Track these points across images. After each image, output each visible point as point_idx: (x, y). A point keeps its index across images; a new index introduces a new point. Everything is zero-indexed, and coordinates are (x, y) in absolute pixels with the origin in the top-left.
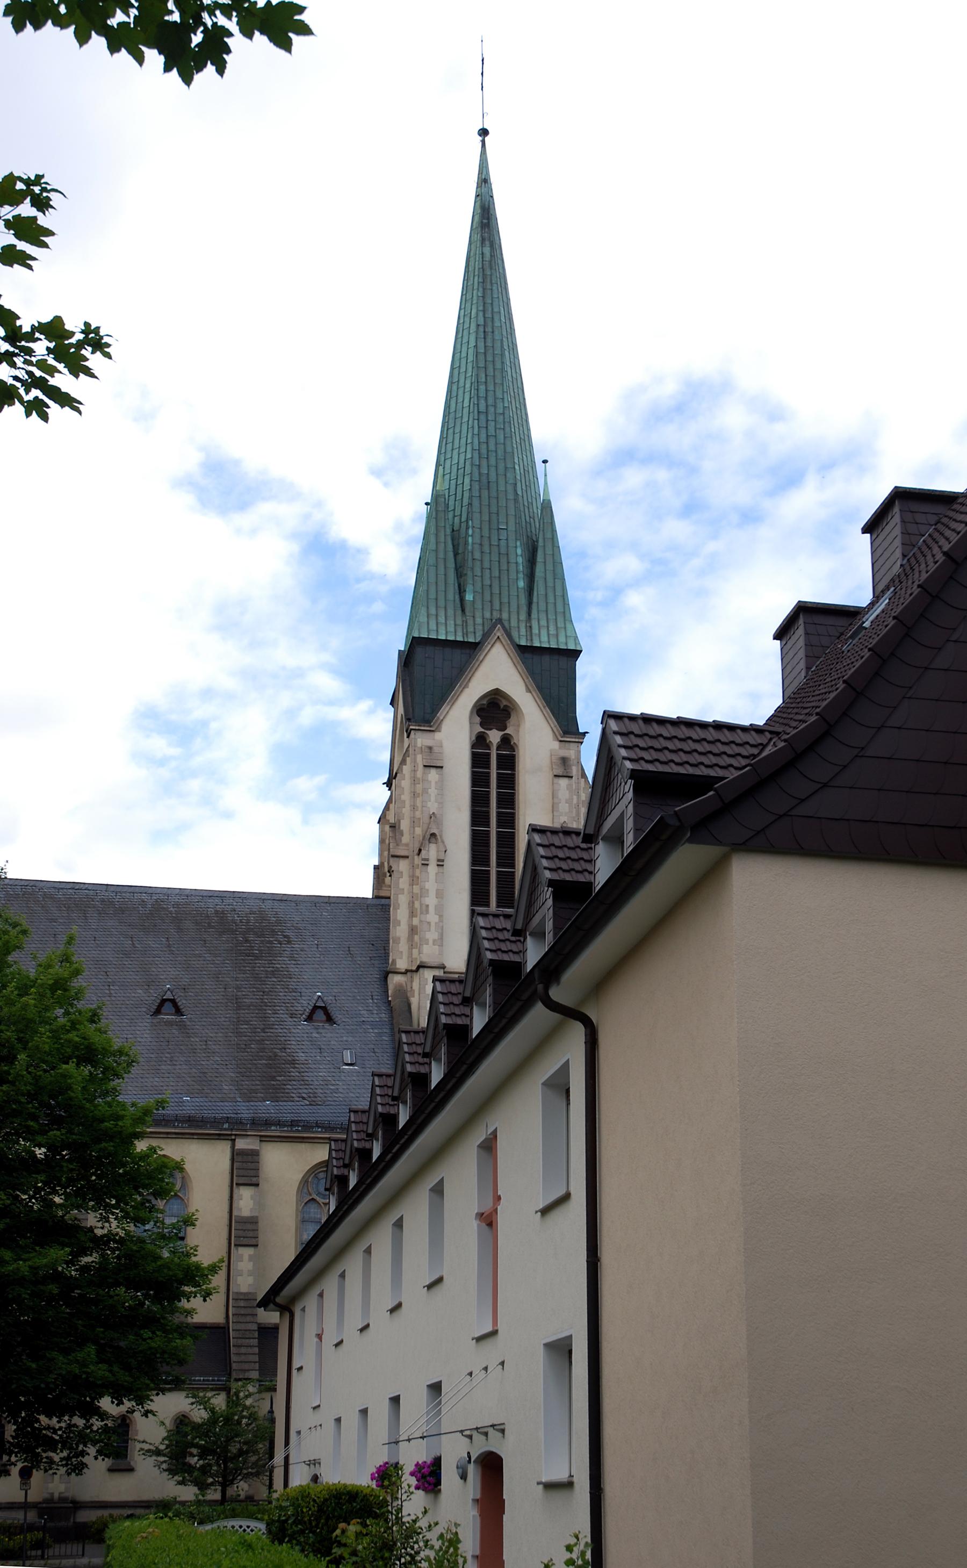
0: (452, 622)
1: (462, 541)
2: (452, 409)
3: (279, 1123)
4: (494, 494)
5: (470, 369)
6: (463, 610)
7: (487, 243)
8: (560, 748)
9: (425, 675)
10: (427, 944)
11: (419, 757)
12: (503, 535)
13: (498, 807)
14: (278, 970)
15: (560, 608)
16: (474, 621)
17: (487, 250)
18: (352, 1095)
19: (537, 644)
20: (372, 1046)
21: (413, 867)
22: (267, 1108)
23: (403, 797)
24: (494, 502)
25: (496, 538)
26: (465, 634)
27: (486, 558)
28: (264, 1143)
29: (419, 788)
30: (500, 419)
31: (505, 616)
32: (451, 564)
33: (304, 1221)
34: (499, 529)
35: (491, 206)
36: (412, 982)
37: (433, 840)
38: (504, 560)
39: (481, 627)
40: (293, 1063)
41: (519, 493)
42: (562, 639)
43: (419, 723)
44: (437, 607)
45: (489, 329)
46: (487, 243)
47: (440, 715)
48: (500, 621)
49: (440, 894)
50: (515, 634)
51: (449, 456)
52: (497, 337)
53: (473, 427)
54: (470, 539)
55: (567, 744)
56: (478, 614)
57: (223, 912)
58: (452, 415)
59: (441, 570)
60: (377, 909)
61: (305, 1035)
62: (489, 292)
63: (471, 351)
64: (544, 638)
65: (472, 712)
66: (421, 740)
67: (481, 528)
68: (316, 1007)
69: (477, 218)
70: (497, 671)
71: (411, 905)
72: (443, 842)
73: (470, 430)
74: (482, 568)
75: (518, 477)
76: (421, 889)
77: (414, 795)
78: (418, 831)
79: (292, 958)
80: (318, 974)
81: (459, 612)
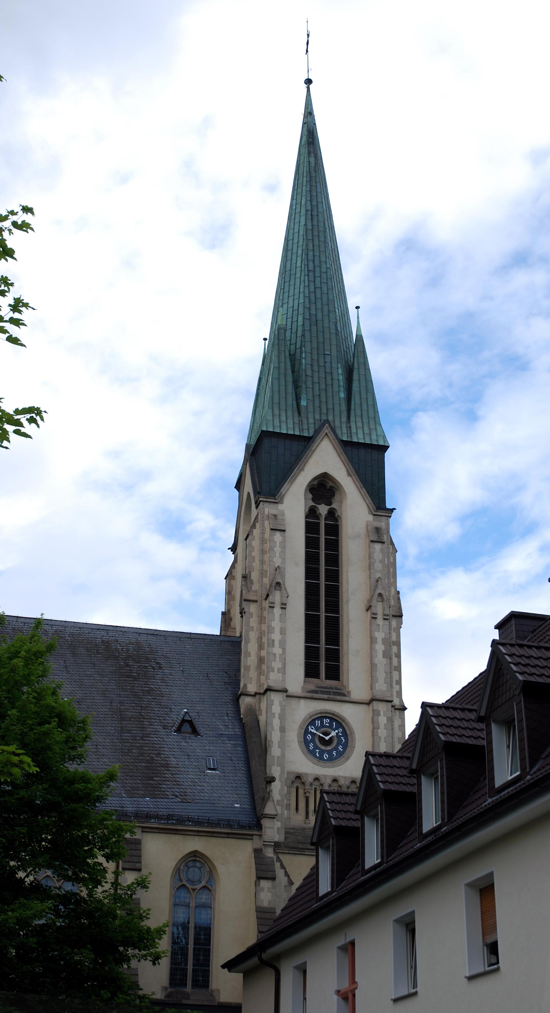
0: (291, 421)
1: (297, 363)
2: (288, 268)
3: (158, 817)
4: (320, 329)
5: (301, 240)
6: (299, 413)
7: (312, 155)
8: (374, 520)
9: (268, 461)
10: (273, 671)
11: (266, 523)
12: (328, 359)
13: (326, 565)
14: (152, 689)
15: (371, 414)
16: (308, 421)
17: (312, 159)
18: (215, 795)
19: (355, 440)
20: (230, 755)
21: (262, 609)
22: (147, 804)
23: (253, 554)
24: (320, 335)
25: (323, 361)
26: (301, 430)
27: (316, 375)
28: (144, 834)
29: (267, 546)
30: (324, 276)
31: (331, 418)
32: (290, 378)
33: (175, 905)
34: (324, 354)
35: (315, 130)
36: (260, 702)
37: (278, 588)
38: (329, 377)
39: (312, 426)
40: (167, 766)
41: (339, 329)
42: (374, 437)
43: (266, 496)
44: (279, 409)
45: (315, 213)
46: (312, 155)
47: (283, 490)
48: (327, 421)
49: (283, 632)
50: (338, 432)
51: (285, 301)
52: (321, 219)
53: (304, 281)
54: (304, 361)
55: (379, 518)
56: (311, 416)
57: (108, 642)
58: (288, 273)
59: (283, 383)
60: (226, 648)
61: (176, 744)
62: (314, 188)
63: (302, 228)
64: (361, 436)
65: (306, 490)
66: (268, 509)
67: (311, 353)
68: (183, 721)
69: (304, 138)
70: (325, 459)
71: (260, 640)
72: (286, 589)
73: (302, 283)
74: (313, 382)
75: (338, 318)
76: (268, 627)
77: (263, 552)
78: (266, 581)
79: (163, 680)
80: (184, 696)
81: (296, 414)
